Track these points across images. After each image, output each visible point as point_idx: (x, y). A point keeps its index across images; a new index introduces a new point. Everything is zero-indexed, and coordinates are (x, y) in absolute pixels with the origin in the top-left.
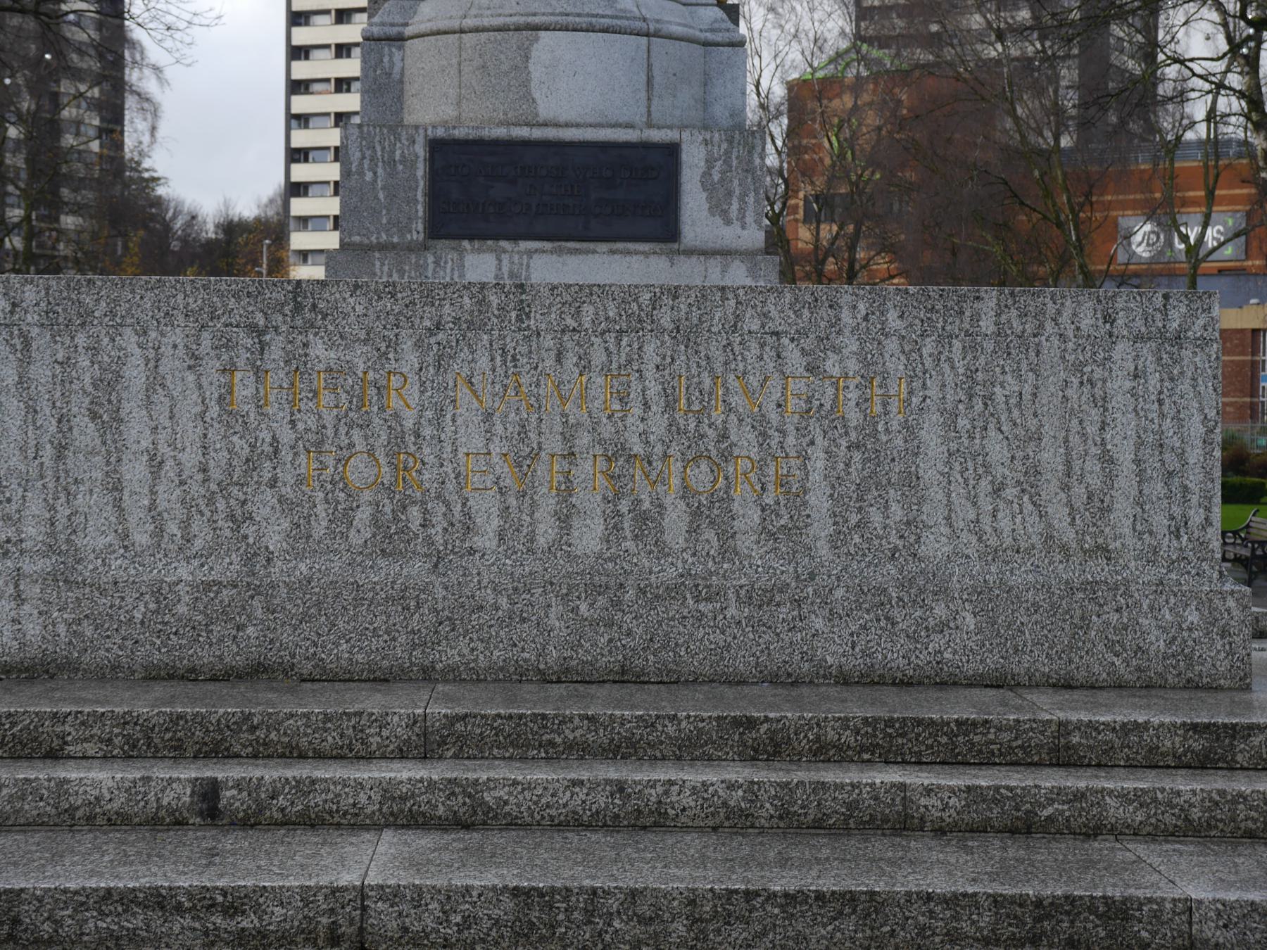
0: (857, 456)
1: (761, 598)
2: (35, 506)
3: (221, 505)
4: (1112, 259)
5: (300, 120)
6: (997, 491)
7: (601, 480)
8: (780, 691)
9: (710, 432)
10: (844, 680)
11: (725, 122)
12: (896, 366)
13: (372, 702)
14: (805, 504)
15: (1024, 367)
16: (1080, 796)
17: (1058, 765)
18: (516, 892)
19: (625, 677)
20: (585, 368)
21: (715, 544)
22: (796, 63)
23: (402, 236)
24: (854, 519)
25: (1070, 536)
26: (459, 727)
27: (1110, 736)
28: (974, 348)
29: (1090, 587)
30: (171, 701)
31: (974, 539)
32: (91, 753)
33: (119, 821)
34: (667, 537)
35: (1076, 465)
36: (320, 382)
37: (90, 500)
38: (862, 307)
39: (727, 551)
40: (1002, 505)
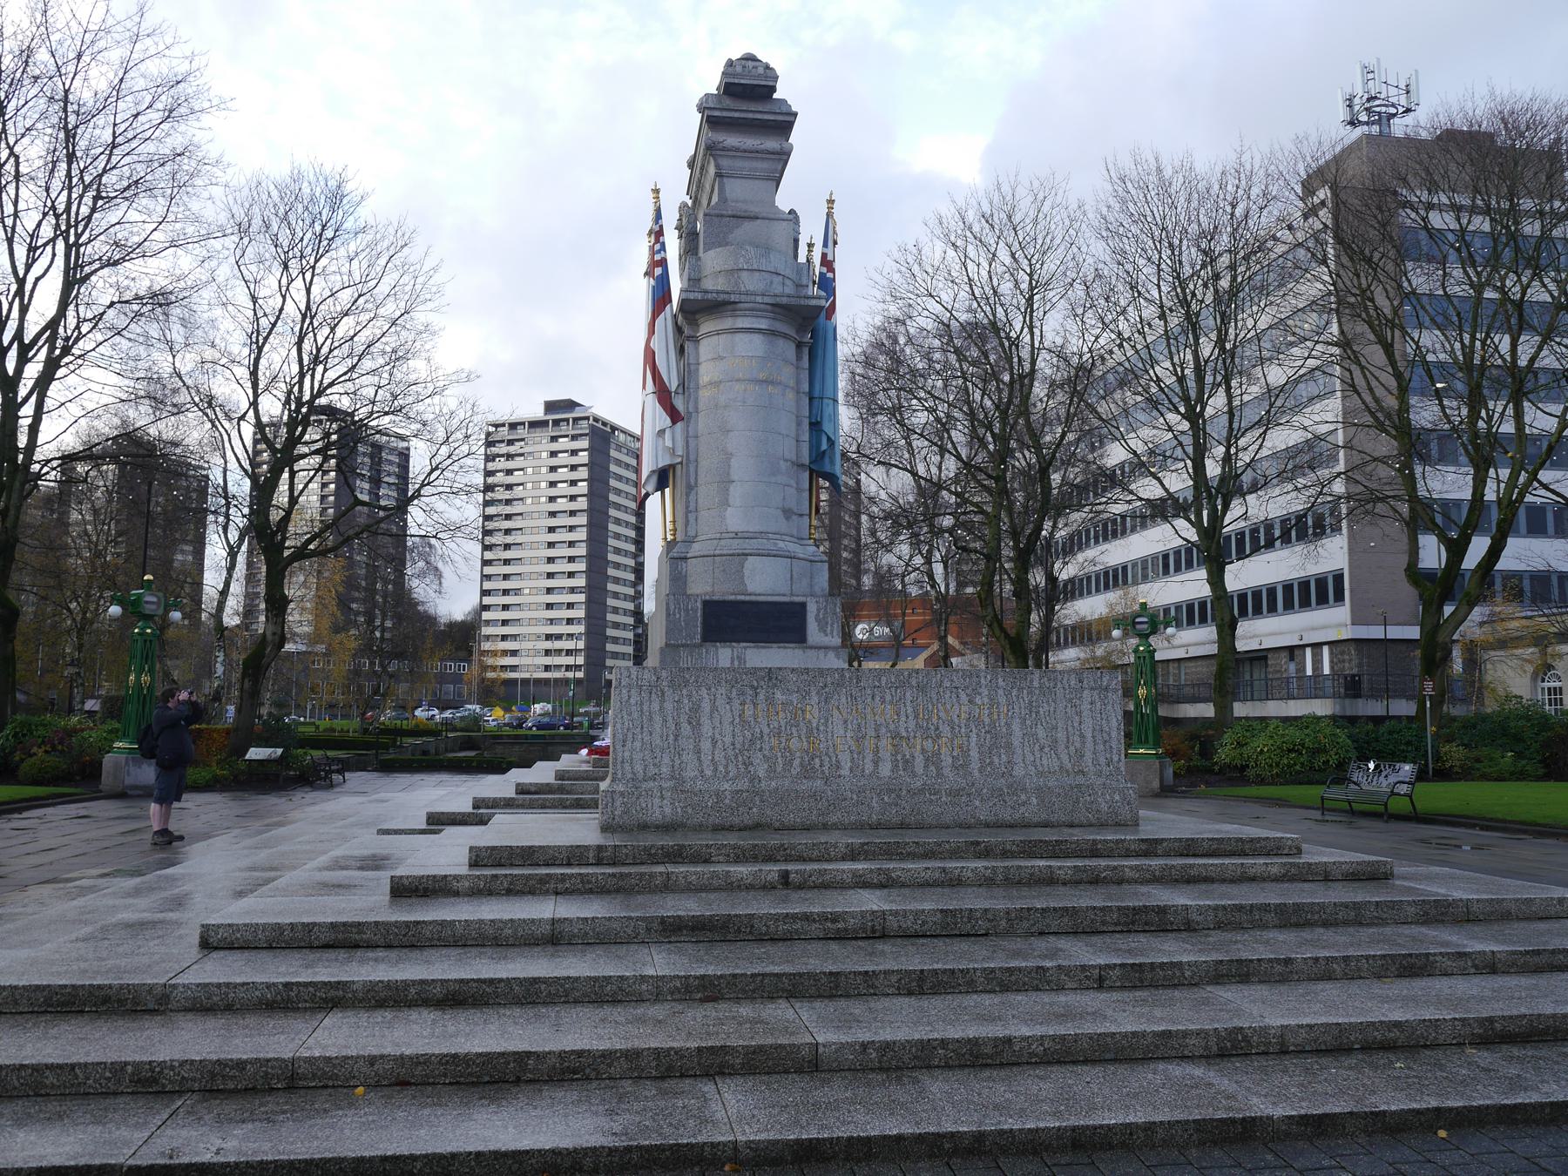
1: (955, 793)
2: (666, 760)
5: (488, 577)
6: (1042, 749)
10: (987, 825)
12: (1003, 700)
16: (1115, 868)
18: (942, 911)
19: (903, 826)
29: (1079, 786)
33: (750, 887)
37: (688, 757)
39: (939, 775)
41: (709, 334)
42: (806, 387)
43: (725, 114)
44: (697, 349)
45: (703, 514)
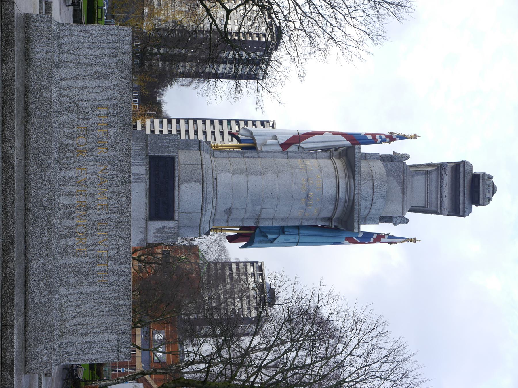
0: (87, 270)
1: (48, 245)
2: (71, 57)
3: (72, 105)
4: (153, 329)
5: (187, 122)
6: (78, 306)
7: (80, 203)
8: (23, 251)
9: (93, 231)
10: (26, 268)
11: (180, 232)
12: (111, 279)
13: (18, 143)
14: (74, 256)
15: (111, 312)
17: (2, 325)
19: (27, 210)
20: (109, 199)
21: (63, 233)
22: (203, 247)
23: (150, 150)
24: (70, 269)
25: (66, 325)
26: (11, 167)
27: (10, 339)
28: (116, 299)
29: (53, 331)
30: (17, 91)
31: (65, 301)
32: (3, 71)
34: (64, 221)
35: (85, 327)
36: (105, 130)
37: (73, 71)
38: (126, 270)
39: (61, 236)
40: (74, 308)
41: (334, 164)
42: (305, 224)
43: (462, 174)
44: (326, 158)
45: (227, 161)
